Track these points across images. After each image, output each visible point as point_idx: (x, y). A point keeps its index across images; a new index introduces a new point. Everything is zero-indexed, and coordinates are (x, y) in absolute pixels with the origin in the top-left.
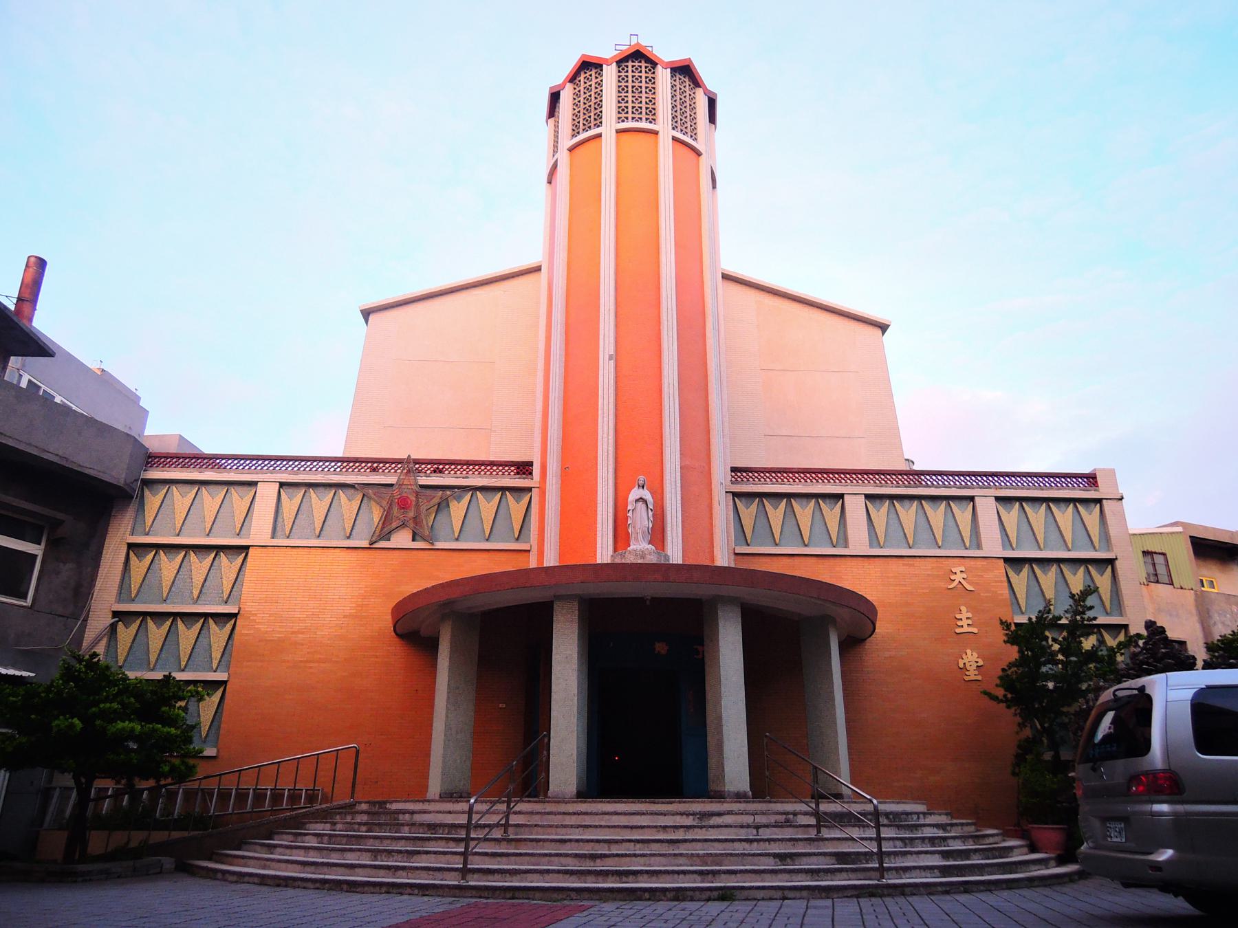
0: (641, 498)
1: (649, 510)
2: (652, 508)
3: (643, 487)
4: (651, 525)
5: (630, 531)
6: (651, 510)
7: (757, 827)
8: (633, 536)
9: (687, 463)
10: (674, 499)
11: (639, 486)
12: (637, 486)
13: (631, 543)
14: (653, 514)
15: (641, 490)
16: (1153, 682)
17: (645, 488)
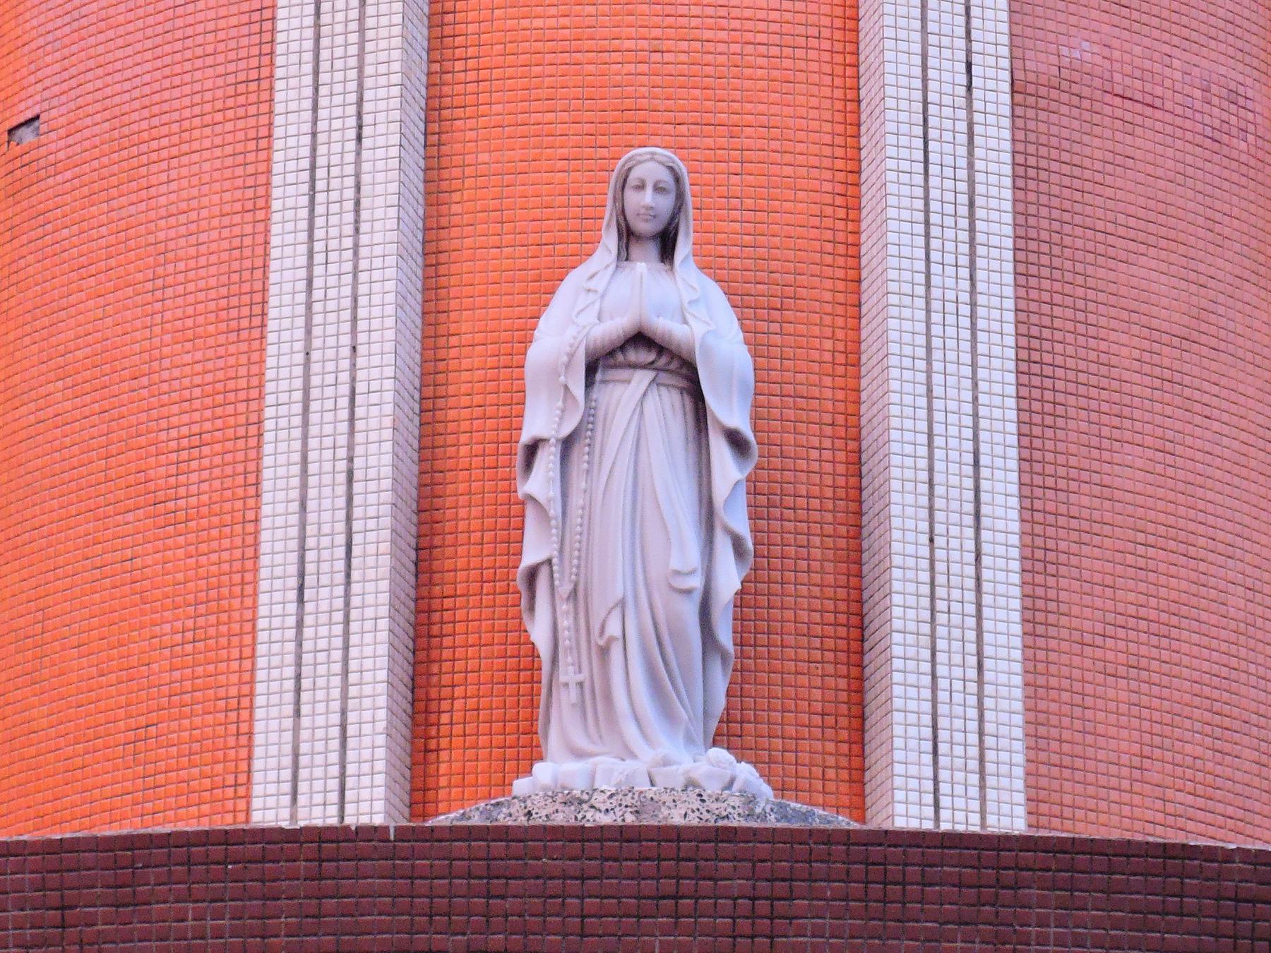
0: (640, 338)
1: (720, 450)
2: (739, 420)
3: (666, 244)
4: (729, 578)
5: (539, 633)
6: (736, 441)
7: (583, 878)
8: (567, 674)
9: (1083, 51)
10: (952, 353)
11: (628, 236)
12: (610, 240)
13: (554, 743)
14: (754, 487)
15: (644, 266)
16: (741, 470)
17: (683, 248)
